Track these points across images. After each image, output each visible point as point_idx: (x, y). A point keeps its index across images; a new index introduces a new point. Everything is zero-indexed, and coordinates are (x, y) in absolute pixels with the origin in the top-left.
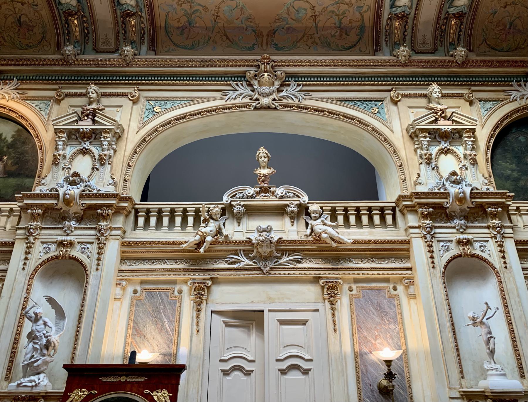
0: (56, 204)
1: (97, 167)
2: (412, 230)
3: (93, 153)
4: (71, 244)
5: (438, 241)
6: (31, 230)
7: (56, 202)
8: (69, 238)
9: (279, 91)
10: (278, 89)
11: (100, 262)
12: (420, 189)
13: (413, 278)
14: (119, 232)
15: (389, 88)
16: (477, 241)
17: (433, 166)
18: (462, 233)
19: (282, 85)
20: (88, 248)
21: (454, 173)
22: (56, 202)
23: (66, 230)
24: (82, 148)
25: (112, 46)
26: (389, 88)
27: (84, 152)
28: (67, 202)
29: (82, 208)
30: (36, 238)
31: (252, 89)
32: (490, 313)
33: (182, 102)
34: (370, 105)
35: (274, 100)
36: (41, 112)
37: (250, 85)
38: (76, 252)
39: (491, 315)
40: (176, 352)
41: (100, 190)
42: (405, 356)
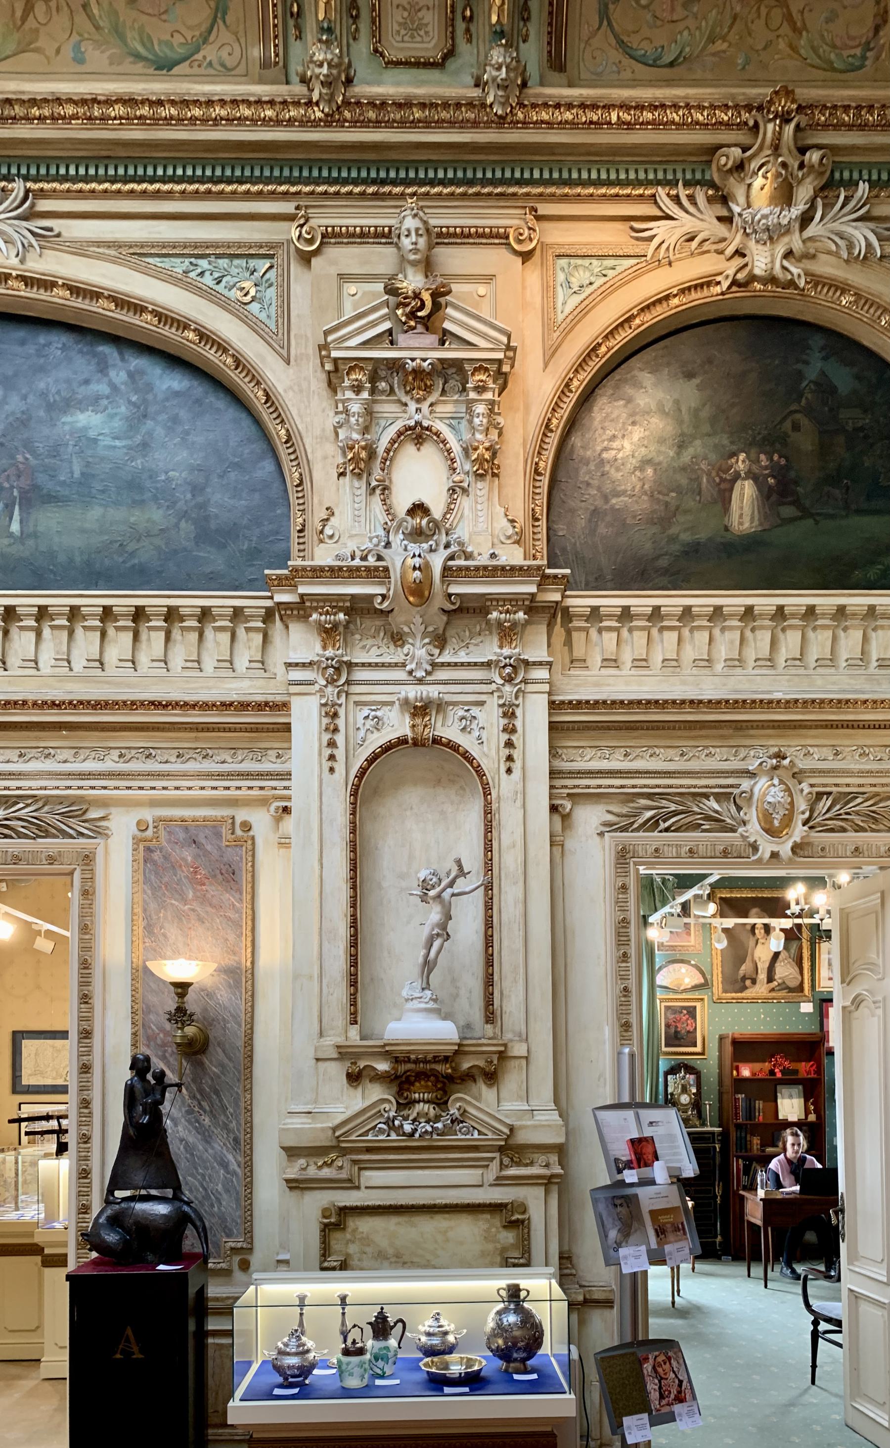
0: (384, 597)
1: (465, 485)
4: (441, 706)
5: (357, 703)
13: (289, 798)
15: (288, 207)
16: (455, 704)
18: (420, 681)
26: (288, 207)
31: (725, 213)
32: (462, 885)
39: (467, 890)
40: (253, 963)
42: (243, 978)
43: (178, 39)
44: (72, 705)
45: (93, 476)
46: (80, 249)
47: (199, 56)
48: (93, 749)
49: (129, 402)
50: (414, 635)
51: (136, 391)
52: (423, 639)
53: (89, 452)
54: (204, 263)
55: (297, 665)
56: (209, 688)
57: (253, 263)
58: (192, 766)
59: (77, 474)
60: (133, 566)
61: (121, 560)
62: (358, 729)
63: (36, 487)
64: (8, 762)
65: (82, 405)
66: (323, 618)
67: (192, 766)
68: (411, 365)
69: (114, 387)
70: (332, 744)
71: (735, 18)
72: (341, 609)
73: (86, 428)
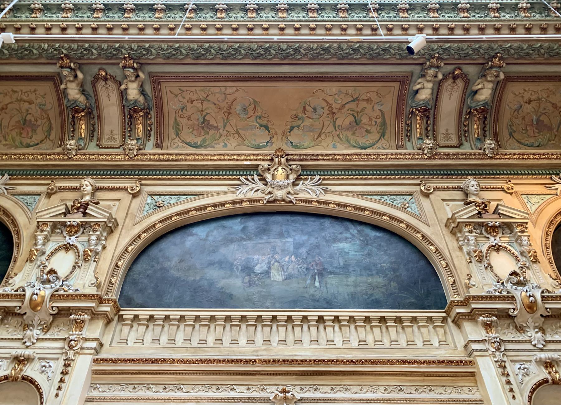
0: (20, 307)
2: (474, 346)
3: (78, 250)
6: (72, 342)
7: (19, 304)
8: (27, 352)
9: (294, 184)
10: (293, 182)
11: (63, 385)
12: (473, 292)
14: (94, 344)
15: (418, 182)
17: (486, 265)
18: (541, 350)
19: (298, 178)
20: (50, 366)
21: (514, 274)
22: (19, 304)
23: (25, 342)
24: (66, 243)
25: (118, 143)
27: (67, 247)
28: (34, 306)
29: (51, 312)
30: (77, 353)
33: (189, 197)
34: (398, 199)
35: (289, 193)
36: (29, 207)
37: (263, 179)
38: (31, 371)
41: (77, 290)
43: (368, 142)
44: (361, 362)
45: (349, 265)
46: (339, 193)
47: (375, 146)
48: (371, 386)
49: (360, 240)
50: (529, 327)
51: (362, 236)
52: (534, 329)
53: (346, 257)
54: (386, 197)
55: (475, 341)
56: (425, 354)
57: (405, 197)
58: (423, 396)
59: (342, 264)
60: (373, 300)
61: (367, 297)
62: (517, 375)
63: (324, 269)
64: (326, 393)
65: (340, 241)
66: (486, 319)
67: (423, 396)
68: (491, 224)
69: (353, 235)
70: (508, 382)
71: (556, 136)
72: (493, 315)
73: (343, 249)
